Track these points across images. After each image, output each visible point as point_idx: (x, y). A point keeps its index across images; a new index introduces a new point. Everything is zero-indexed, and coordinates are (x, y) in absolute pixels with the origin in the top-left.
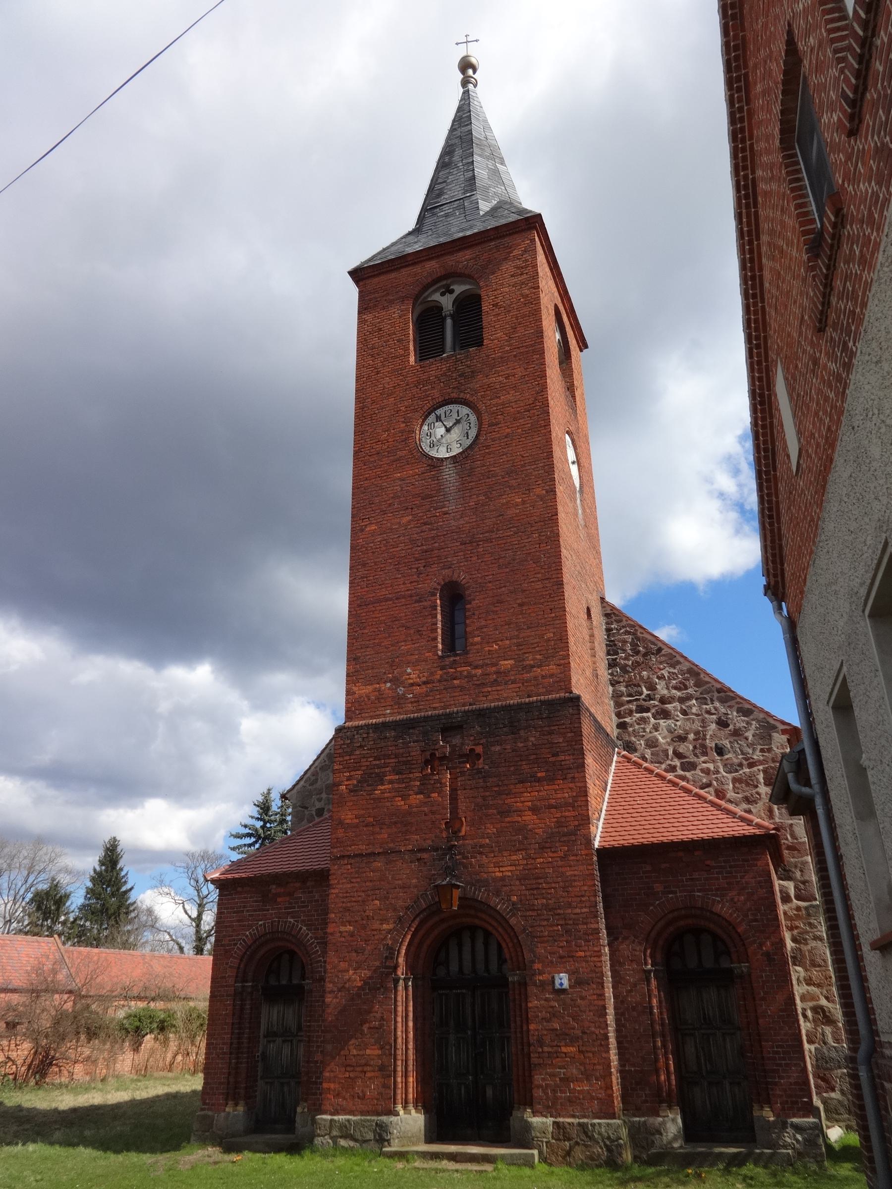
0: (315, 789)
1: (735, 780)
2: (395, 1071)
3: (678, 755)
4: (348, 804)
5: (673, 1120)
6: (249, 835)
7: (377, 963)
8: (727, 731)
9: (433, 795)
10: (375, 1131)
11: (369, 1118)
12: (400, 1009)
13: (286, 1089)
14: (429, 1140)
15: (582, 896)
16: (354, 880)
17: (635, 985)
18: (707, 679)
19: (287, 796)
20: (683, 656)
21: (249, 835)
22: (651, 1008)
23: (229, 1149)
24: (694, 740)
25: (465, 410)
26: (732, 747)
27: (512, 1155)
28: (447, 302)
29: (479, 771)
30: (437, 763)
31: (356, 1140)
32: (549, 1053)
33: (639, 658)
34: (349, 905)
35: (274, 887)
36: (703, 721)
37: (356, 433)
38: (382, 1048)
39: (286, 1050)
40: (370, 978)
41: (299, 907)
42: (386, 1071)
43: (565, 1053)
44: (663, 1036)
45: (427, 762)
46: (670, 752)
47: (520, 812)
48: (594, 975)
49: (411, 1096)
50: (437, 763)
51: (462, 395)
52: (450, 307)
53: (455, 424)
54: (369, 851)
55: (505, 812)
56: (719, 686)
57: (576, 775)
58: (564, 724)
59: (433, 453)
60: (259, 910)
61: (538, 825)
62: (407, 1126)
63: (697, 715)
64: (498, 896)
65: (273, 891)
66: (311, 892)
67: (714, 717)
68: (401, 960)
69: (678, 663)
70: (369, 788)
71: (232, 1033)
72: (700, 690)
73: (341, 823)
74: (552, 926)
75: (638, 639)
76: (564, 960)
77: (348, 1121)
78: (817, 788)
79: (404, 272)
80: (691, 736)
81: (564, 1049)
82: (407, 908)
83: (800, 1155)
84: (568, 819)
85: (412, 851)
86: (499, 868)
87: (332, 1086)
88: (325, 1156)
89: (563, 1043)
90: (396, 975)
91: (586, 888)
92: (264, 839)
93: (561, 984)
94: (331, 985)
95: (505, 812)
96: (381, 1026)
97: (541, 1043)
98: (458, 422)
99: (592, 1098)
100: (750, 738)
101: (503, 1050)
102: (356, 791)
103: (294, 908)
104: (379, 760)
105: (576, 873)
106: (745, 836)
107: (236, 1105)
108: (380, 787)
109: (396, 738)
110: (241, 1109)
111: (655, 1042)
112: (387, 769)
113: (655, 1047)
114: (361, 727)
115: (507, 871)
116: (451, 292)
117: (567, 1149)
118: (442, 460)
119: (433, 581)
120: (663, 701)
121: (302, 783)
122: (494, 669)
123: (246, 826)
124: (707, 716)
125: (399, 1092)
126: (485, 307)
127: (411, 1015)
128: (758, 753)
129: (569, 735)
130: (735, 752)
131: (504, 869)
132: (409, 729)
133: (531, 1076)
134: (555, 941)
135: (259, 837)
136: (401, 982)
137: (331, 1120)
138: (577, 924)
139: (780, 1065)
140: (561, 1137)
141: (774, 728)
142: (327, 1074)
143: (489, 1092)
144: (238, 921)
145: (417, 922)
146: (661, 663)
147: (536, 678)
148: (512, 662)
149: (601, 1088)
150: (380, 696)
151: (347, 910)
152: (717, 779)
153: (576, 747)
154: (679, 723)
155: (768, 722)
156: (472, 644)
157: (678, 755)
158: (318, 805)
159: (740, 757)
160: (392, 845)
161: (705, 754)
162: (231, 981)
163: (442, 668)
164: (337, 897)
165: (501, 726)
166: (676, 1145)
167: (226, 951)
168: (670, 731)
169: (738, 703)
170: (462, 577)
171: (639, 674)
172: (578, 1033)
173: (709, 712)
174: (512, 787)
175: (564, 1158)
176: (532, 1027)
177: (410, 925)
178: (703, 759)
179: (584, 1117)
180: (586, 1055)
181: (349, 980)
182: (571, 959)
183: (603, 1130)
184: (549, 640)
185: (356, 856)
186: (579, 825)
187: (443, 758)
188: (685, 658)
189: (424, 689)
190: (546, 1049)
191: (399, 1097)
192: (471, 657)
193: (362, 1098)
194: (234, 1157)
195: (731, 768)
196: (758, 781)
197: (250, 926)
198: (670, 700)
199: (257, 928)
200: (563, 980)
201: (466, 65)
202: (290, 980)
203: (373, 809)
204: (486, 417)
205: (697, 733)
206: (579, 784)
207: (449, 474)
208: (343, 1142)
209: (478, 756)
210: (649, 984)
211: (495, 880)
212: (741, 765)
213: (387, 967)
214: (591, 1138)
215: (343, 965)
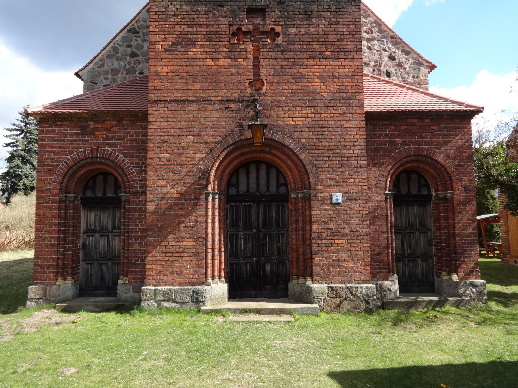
0: (103, 71)
2: (206, 256)
4: (164, 60)
6: (17, 130)
7: (192, 182)
9: (239, 60)
10: (192, 296)
11: (186, 287)
12: (210, 214)
13: (104, 267)
15: (355, 142)
16: (171, 120)
18: (385, 29)
19: (80, 73)
20: (372, 13)
24: (374, 66)
26: (396, 73)
27: (302, 309)
29: (278, 46)
31: (177, 302)
32: (325, 243)
34: (166, 138)
35: (92, 123)
39: (103, 242)
40: (185, 192)
41: (115, 139)
42: (200, 256)
43: (338, 244)
45: (234, 34)
48: (360, 194)
54: (184, 98)
56: (392, 34)
57: (355, 57)
58: (347, 18)
60: (79, 140)
61: (325, 90)
62: (216, 292)
65: (91, 126)
66: (127, 129)
67: (388, 53)
69: (369, 16)
70: (183, 50)
71: (59, 230)
73: (157, 75)
74: (331, 161)
76: (340, 184)
77: (170, 290)
81: (337, 241)
84: (347, 88)
86: (291, 121)
87: (154, 266)
88: (152, 314)
89: (336, 238)
90: (207, 190)
91: (358, 136)
92: (26, 133)
93: (337, 200)
94: (152, 196)
95: (298, 79)
96: (195, 226)
97: (320, 237)
99: (355, 272)
100: (407, 69)
101: (279, 242)
102: (171, 50)
103: (112, 140)
104: (192, 28)
105: (351, 126)
107: (65, 279)
108: (193, 50)
110: (69, 282)
112: (199, 36)
115: (299, 121)
117: (339, 302)
121: (91, 65)
123: (14, 125)
124: (383, 52)
127: (217, 218)
128: (411, 78)
129: (351, 26)
130: (397, 76)
131: (296, 119)
132: (219, 6)
133: (311, 258)
134: (334, 171)
135: (22, 131)
136: (211, 195)
137: (155, 290)
138: (351, 161)
139: (465, 250)
140: (334, 296)
142: (150, 259)
143: (268, 268)
144: (60, 147)
145: (224, 154)
149: (361, 265)
153: (356, 36)
155: (418, 60)
158: (105, 82)
159: (400, 79)
160: (203, 95)
162: (55, 192)
165: (297, 13)
167: (49, 170)
169: (403, 47)
172: (347, 231)
173: (384, 50)
174: (305, 60)
177: (219, 156)
179: (349, 283)
180: (352, 245)
182: (345, 184)
183: (364, 291)
185: (171, 101)
186: (356, 92)
190: (324, 241)
193: (180, 274)
194: (72, 317)
197: (71, 152)
199: (78, 154)
200: (338, 197)
202: (105, 193)
203: (187, 66)
205: (376, 62)
206: (357, 64)
208: (166, 304)
209: (278, 34)
211: (289, 127)
215: (162, 182)
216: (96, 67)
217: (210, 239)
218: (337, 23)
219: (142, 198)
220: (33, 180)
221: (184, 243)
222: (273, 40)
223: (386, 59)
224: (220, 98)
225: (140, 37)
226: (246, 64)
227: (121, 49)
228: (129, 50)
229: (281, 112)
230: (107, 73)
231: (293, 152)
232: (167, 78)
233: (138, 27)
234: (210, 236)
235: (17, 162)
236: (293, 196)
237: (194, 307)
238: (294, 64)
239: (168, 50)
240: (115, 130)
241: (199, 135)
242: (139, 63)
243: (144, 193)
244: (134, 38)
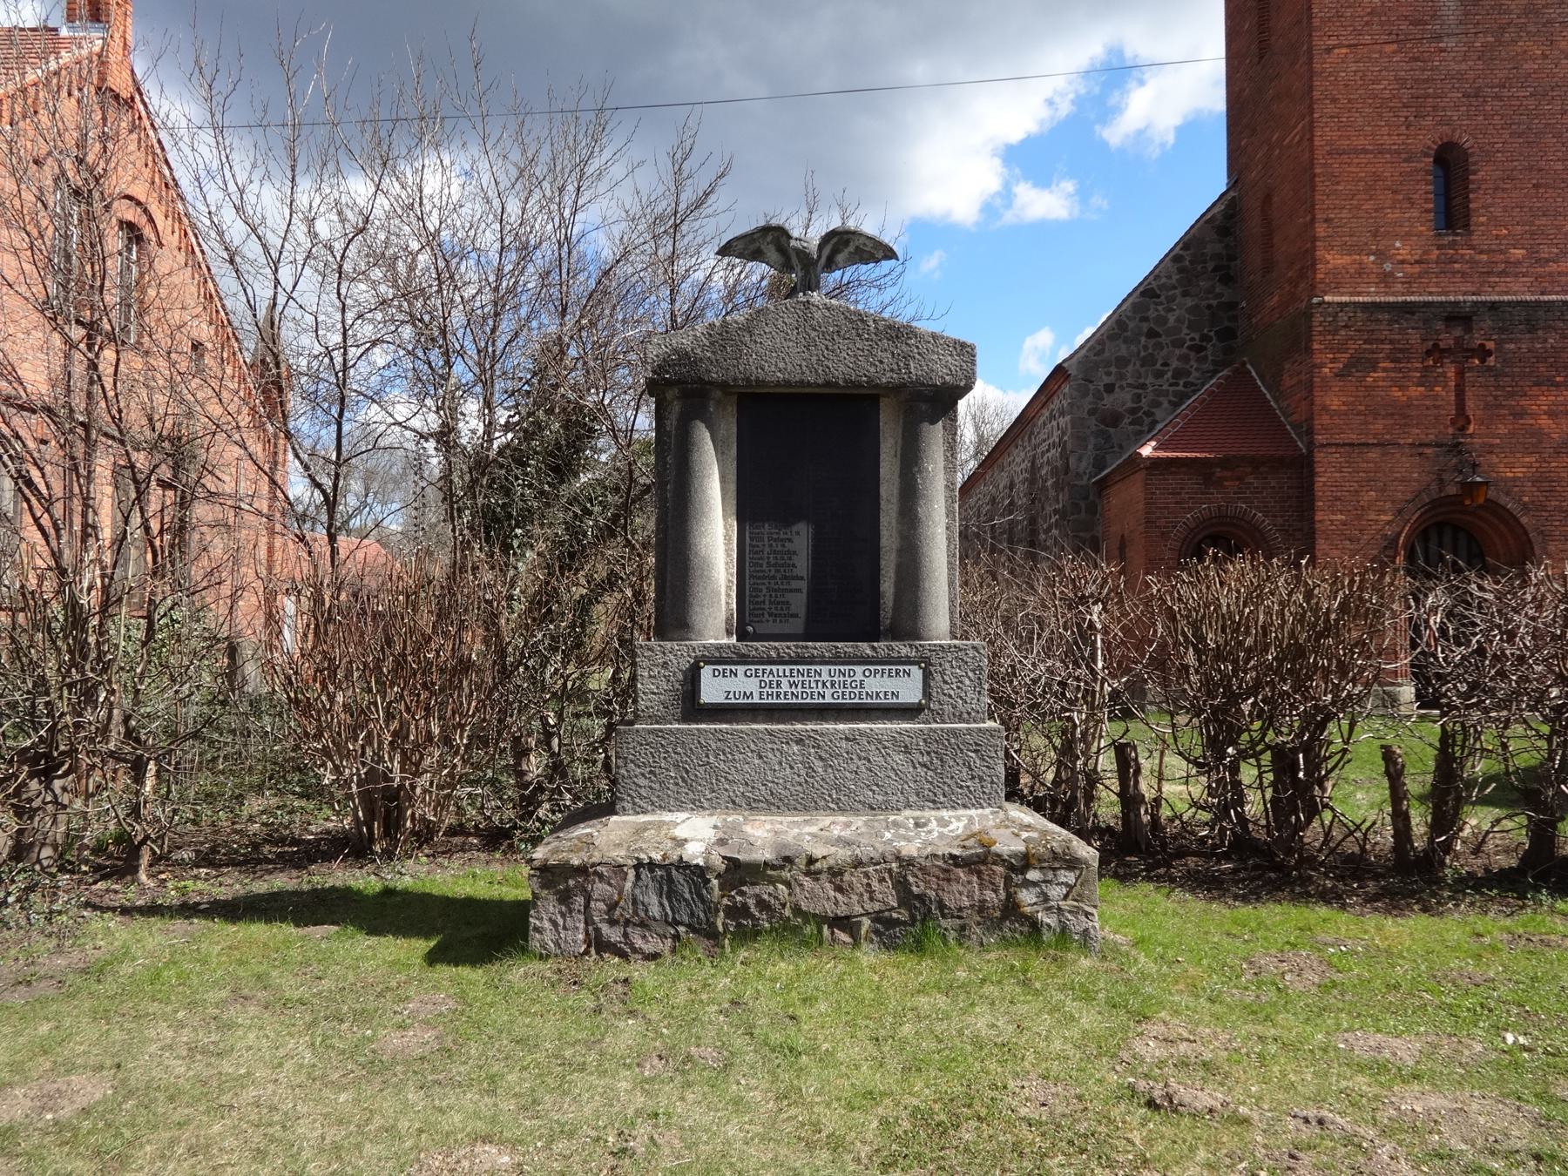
29: (1490, 369)
30: (1437, 355)
45: (1429, 353)
47: (1535, 416)
55: (1519, 414)
73: (1325, 408)
95: (1519, 414)
109: (1390, 323)
114: (1346, 304)
115: (1519, 471)
119: (1427, 137)
147: (1550, 274)
150: (1361, 271)
151: (1337, 499)
158: (1107, 380)
170: (1466, 140)
187: (1448, 350)
189: (1417, 269)
192: (1476, 239)
197: (1190, 509)
209: (1490, 353)
211: (1506, 480)
216: (1091, 354)
222: (1483, 361)
227: (1131, 325)
228: (1145, 326)
230: (1108, 364)
232: (1338, 413)
238: (1512, 395)
239: (1340, 375)
240: (1250, 479)
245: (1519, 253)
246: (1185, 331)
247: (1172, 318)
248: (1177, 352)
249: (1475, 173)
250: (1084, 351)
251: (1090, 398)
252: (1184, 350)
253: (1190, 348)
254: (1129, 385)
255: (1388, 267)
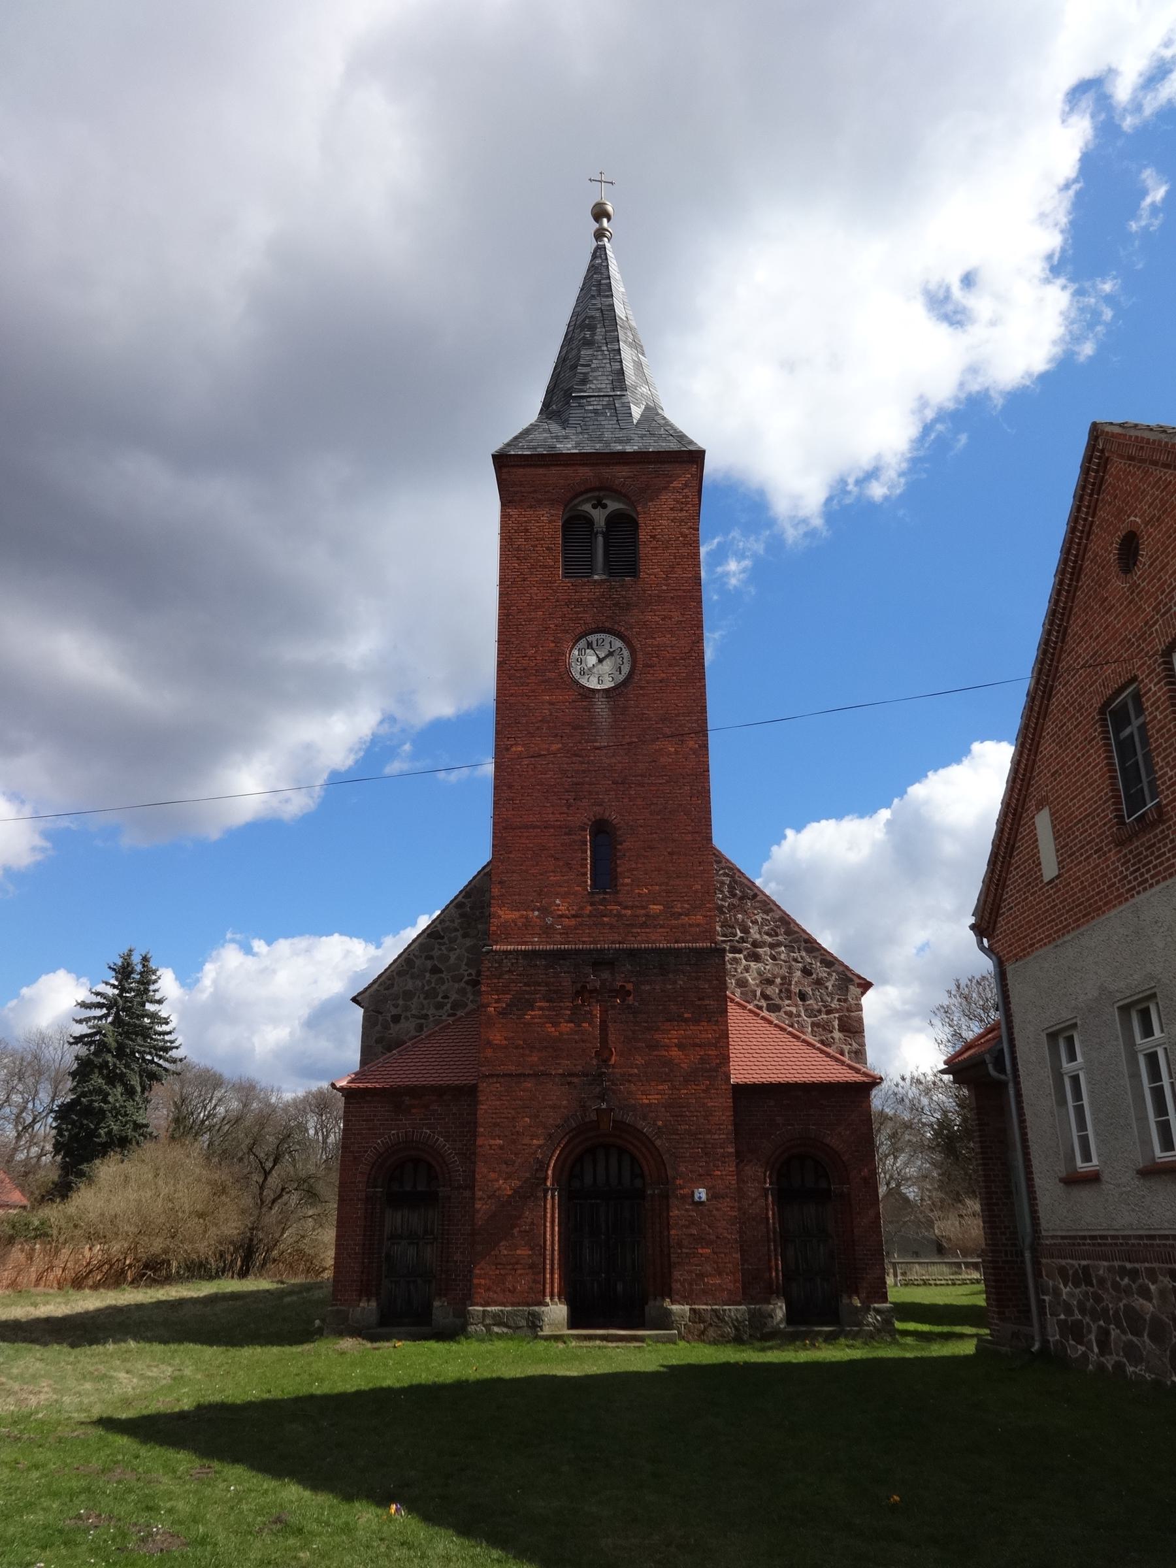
1: (813, 1024)
2: (544, 1269)
3: (765, 996)
5: (781, 1308)
6: (100, 1006)
7: (528, 1175)
8: (810, 979)
10: (527, 1320)
12: (549, 1215)
14: (569, 1328)
17: (756, 1200)
18: (796, 929)
19: (359, 998)
21: (100, 1006)
22: (768, 1219)
23: (373, 1338)
25: (618, 643)
28: (599, 516)
29: (629, 1007)
30: (586, 995)
33: (735, 901)
36: (790, 968)
37: (500, 641)
38: (532, 1249)
40: (521, 1187)
42: (537, 1269)
44: (775, 1242)
45: (578, 993)
46: (758, 993)
47: (667, 1048)
49: (556, 1290)
50: (586, 995)
51: (616, 627)
52: (603, 523)
53: (607, 656)
59: (583, 681)
63: (785, 961)
64: (644, 1120)
68: (550, 1172)
69: (771, 910)
72: (790, 938)
73: (489, 1043)
75: (736, 882)
78: (1010, 1076)
79: (554, 470)
80: (778, 981)
81: (700, 1251)
82: (558, 1126)
83: (879, 1331)
85: (563, 1075)
87: (483, 1282)
97: (680, 1246)
98: (611, 654)
99: (723, 1290)
106: (856, 1083)
107: (368, 1301)
110: (374, 1304)
111: (769, 1246)
113: (769, 1249)
114: (510, 952)
115: (654, 1099)
116: (604, 506)
118: (593, 691)
120: (755, 944)
121: (376, 986)
122: (643, 912)
125: (548, 1286)
126: (643, 536)
130: (816, 999)
133: (670, 1273)
141: (851, 980)
143: (620, 1287)
146: (755, 908)
148: (661, 907)
151: (496, 1125)
152: (798, 1022)
154: (768, 967)
156: (623, 885)
157: (765, 996)
158: (394, 1011)
161: (789, 998)
163: (592, 904)
164: (486, 1112)
166: (782, 1326)
168: (760, 974)
170: (614, 817)
171: (735, 916)
173: (796, 960)
175: (699, 1336)
176: (673, 1232)
178: (787, 1002)
181: (499, 1189)
184: (696, 892)
185: (505, 1075)
188: (779, 907)
189: (573, 922)
191: (548, 1291)
193: (513, 1291)
195: (811, 1013)
196: (833, 1027)
198: (761, 944)
200: (702, 1194)
201: (600, 213)
204: (640, 655)
207: (601, 708)
208: (496, 1329)
209: (628, 993)
210: (767, 1200)
211: (642, 1105)
212: (820, 1011)
213: (537, 1179)
214: (723, 1320)
215: (493, 1175)
217: (548, 1247)
218: (697, 979)
219: (467, 1193)
220: (127, 1122)
221: (518, 1252)
223: (799, 973)
224: (561, 1071)
225: (444, 944)
226: (591, 1029)
227: (418, 962)
228: (429, 964)
229: (633, 1087)
231: (647, 1137)
233: (443, 929)
234: (548, 1243)
235: (97, 1080)
236: (649, 1192)
237: (529, 1333)
239: (503, 1013)
241: (537, 1117)
242: (443, 983)
243: (472, 1188)
244: (437, 946)
245: (656, 908)
246: (464, 967)
247: (453, 957)
248: (456, 985)
249: (621, 844)
250: (376, 986)
251: (379, 1028)
252: (462, 984)
253: (467, 983)
254: (413, 1016)
255: (549, 920)
